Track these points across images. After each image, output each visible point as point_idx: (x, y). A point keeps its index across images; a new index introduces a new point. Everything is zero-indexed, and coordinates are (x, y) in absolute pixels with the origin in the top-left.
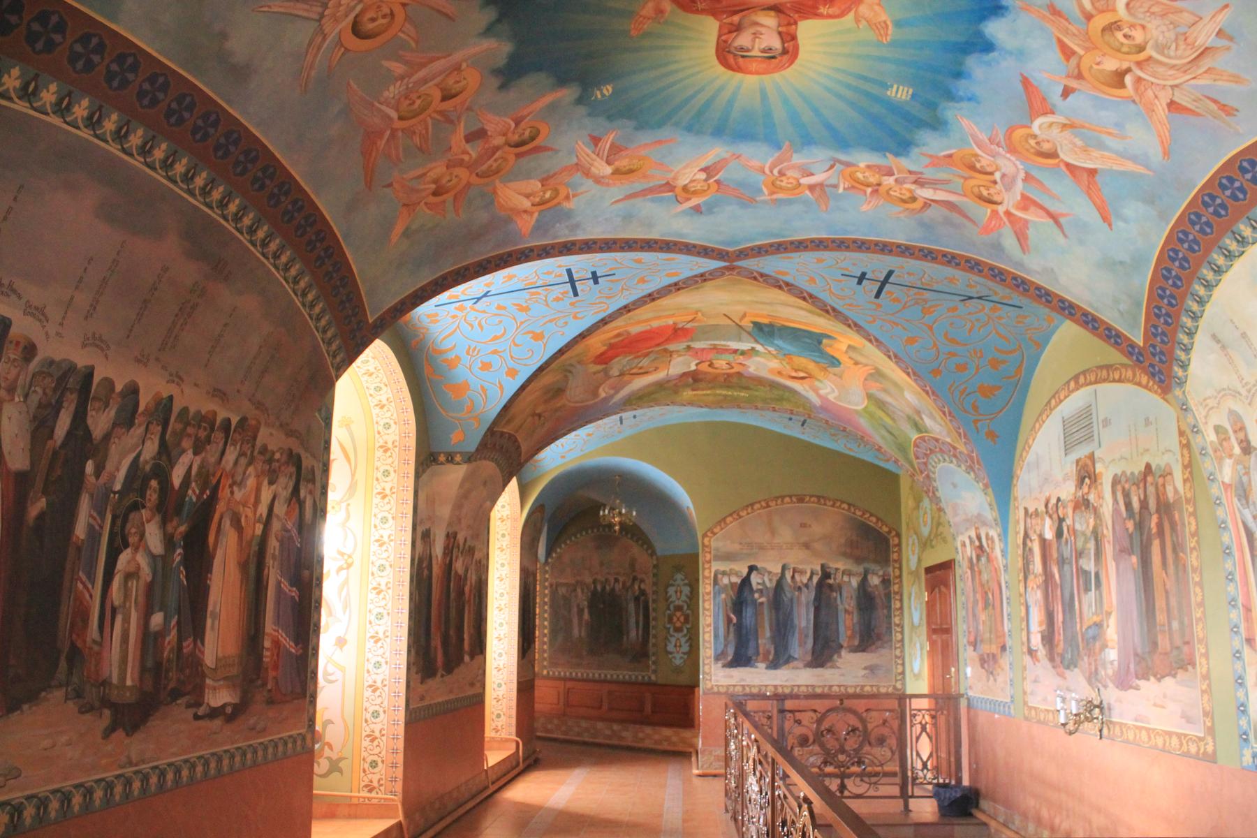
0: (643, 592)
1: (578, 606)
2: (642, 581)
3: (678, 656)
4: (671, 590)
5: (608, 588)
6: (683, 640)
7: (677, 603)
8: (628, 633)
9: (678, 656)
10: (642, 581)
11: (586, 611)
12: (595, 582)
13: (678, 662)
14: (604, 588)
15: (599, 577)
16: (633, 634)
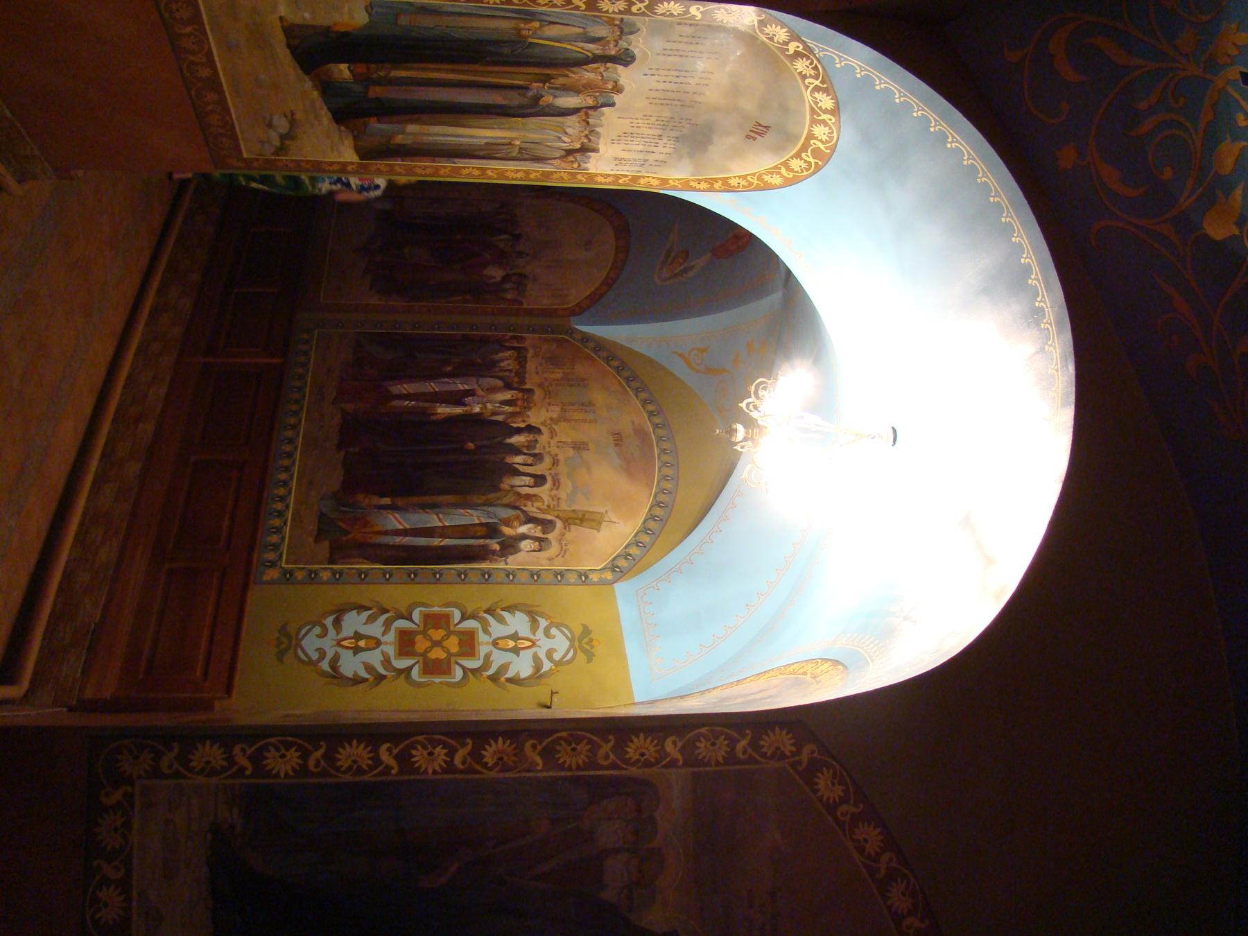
0: (509, 546)
1: (471, 393)
2: (542, 543)
3: (544, 644)
4: (351, 665)
5: (519, 459)
6: (497, 629)
7: (391, 650)
8: (393, 508)
9: (328, 644)
10: (542, 543)
11: (459, 410)
12: (530, 429)
13: (311, 643)
14: (517, 451)
15: (543, 439)
16: (395, 521)
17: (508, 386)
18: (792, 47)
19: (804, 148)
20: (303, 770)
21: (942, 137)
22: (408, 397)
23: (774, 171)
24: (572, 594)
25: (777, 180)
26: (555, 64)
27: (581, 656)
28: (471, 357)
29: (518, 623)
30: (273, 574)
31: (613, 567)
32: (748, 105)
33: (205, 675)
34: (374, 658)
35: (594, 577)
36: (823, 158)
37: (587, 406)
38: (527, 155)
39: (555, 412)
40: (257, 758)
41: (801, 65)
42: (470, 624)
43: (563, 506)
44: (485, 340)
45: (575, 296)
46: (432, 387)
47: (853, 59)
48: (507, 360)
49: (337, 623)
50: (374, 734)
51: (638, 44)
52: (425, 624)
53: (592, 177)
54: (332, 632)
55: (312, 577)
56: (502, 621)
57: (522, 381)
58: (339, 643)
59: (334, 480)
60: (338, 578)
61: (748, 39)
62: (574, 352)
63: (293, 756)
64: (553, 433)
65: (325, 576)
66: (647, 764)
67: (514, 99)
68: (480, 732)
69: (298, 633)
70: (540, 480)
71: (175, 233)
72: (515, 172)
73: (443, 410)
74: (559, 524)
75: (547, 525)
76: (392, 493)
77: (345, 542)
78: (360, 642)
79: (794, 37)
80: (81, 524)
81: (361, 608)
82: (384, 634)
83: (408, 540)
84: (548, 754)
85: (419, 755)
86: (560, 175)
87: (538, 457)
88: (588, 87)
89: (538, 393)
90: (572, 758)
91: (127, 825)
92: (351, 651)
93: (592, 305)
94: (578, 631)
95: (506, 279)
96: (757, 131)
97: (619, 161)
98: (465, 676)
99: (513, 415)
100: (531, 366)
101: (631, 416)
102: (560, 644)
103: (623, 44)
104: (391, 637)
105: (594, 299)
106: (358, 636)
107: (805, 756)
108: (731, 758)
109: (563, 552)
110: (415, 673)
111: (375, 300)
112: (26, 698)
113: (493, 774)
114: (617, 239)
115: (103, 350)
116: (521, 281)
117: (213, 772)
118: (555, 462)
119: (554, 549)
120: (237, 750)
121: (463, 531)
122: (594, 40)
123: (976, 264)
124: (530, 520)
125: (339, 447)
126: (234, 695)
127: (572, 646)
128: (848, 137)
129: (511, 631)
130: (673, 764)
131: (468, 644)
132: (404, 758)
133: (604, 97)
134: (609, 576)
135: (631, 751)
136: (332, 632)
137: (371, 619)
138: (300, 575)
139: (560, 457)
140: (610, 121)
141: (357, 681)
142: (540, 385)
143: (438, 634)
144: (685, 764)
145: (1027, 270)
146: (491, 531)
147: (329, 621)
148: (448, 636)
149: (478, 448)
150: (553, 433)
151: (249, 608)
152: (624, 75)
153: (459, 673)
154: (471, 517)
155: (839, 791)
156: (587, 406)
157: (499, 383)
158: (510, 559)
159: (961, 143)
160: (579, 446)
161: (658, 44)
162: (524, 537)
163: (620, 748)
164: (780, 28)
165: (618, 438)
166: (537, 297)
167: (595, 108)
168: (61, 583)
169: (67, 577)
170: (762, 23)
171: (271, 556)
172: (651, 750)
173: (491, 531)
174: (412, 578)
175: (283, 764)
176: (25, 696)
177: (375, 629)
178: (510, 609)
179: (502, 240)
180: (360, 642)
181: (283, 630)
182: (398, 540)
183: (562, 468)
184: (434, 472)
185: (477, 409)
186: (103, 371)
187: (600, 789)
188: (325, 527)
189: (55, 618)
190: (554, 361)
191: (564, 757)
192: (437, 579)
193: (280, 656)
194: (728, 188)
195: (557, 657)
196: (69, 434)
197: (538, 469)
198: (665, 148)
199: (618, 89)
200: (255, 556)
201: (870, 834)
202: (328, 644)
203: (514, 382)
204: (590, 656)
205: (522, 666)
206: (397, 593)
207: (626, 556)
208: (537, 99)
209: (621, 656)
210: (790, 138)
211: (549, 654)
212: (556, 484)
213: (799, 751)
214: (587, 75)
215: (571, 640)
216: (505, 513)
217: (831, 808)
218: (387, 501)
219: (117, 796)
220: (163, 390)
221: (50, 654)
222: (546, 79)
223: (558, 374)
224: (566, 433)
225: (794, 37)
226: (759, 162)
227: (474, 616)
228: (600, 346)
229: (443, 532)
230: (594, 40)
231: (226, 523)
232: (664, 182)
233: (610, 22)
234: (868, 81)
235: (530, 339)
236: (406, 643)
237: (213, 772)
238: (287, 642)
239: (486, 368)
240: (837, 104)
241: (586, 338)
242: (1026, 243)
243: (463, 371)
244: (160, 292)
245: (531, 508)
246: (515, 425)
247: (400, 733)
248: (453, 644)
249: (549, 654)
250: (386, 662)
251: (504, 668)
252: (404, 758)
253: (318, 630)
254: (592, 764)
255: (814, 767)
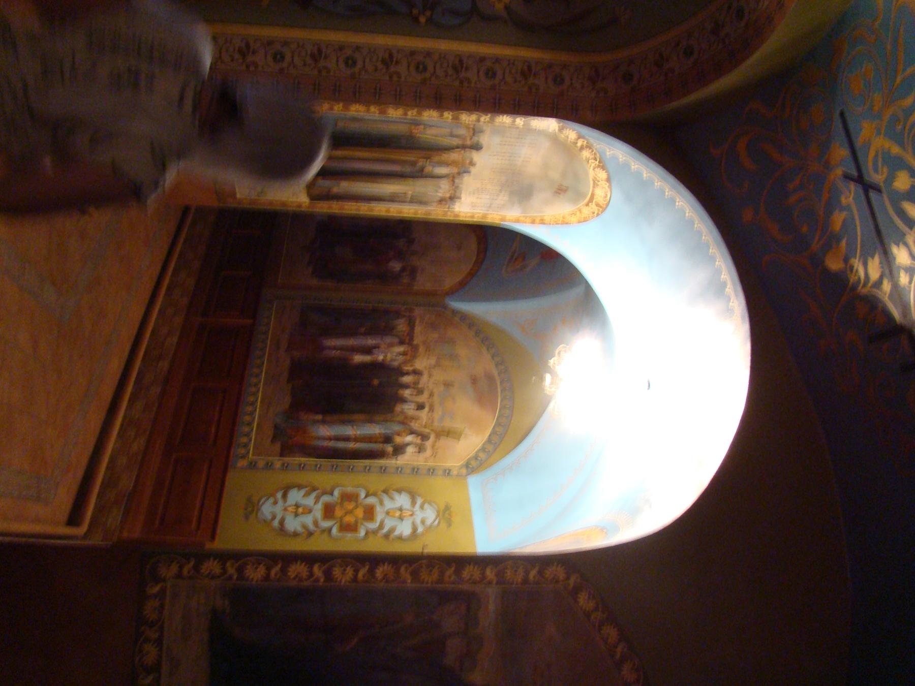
0: (399, 450)
1: (377, 347)
2: (421, 449)
3: (419, 516)
4: (292, 524)
8: (324, 422)
9: (278, 509)
12: (416, 373)
13: (267, 509)
14: (406, 386)
15: (424, 379)
16: (324, 431)
17: (402, 343)
18: (580, 143)
19: (591, 200)
20: (267, 578)
21: (673, 201)
22: (335, 348)
23: (574, 214)
24: (438, 482)
25: (574, 219)
26: (433, 150)
27: (443, 525)
28: (378, 322)
29: (403, 500)
30: (242, 463)
31: (467, 465)
32: (555, 175)
33: (198, 528)
34: (308, 520)
35: (454, 472)
36: (602, 208)
37: (453, 357)
38: (415, 200)
39: (433, 361)
40: (240, 570)
41: (586, 154)
42: (371, 500)
43: (436, 424)
44: (387, 312)
45: (449, 283)
46: (351, 342)
47: (618, 152)
48: (401, 325)
49: (285, 496)
50: (310, 559)
51: (484, 139)
52: (342, 499)
53: (457, 216)
54: (280, 502)
55: (269, 466)
56: (392, 498)
57: (412, 339)
58: (285, 509)
59: (287, 401)
60: (285, 467)
61: (554, 139)
62: (446, 319)
63: (261, 571)
64: (430, 376)
65: (278, 464)
66: (475, 583)
67: (408, 169)
68: (374, 560)
69: (259, 501)
70: (421, 407)
71: (183, 235)
72: (408, 211)
73: (358, 358)
74: (432, 437)
75: (425, 437)
76: (324, 412)
77: (290, 443)
78: (298, 509)
79: (580, 137)
80: (122, 425)
81: (300, 487)
82: (315, 503)
83: (332, 444)
84: (415, 574)
85: (337, 572)
86: (437, 213)
87: (420, 392)
88: (454, 163)
89: (421, 349)
90: (429, 578)
91: (162, 607)
92: (293, 512)
93: (461, 288)
94: (442, 507)
95: (403, 269)
96: (560, 190)
97: (473, 205)
98: (366, 534)
99: (405, 362)
100: (418, 329)
101: (484, 364)
102: (430, 515)
103: (475, 139)
104: (320, 506)
105: (462, 285)
106: (297, 506)
107: (572, 581)
108: (525, 581)
109: (434, 455)
110: (335, 531)
111: (315, 282)
112: (85, 536)
113: (382, 584)
114: (479, 243)
115: (137, 313)
116: (413, 272)
117: (213, 577)
118: (431, 395)
119: (428, 452)
120: (228, 564)
121: (370, 439)
122: (457, 136)
123: (699, 276)
124: (412, 432)
125: (288, 381)
126: (217, 539)
127: (438, 516)
128: (617, 197)
129: (398, 505)
130: (490, 583)
131: (370, 513)
132: (328, 574)
133: (464, 169)
134: (464, 471)
135: (466, 574)
136: (280, 502)
137: (307, 495)
138: (261, 464)
139: (435, 391)
140: (468, 182)
141: (296, 534)
142: (424, 342)
143: (350, 506)
144: (497, 583)
145: (724, 285)
146: (388, 439)
147: (279, 495)
148: (356, 507)
149: (380, 384)
150: (430, 376)
151: (227, 483)
152: (476, 156)
153: (362, 533)
154: (375, 430)
155: (592, 605)
156: (453, 357)
157: (396, 340)
158: (400, 457)
159: (683, 204)
160: (448, 385)
161: (497, 140)
162: (408, 444)
163: (458, 572)
164: (572, 132)
165: (474, 381)
166: (423, 283)
167: (459, 174)
168: (108, 464)
169: (112, 460)
170: (561, 130)
171: (242, 451)
172: (477, 574)
173: (388, 439)
174: (334, 469)
175: (255, 574)
176: (85, 534)
177: (310, 501)
178: (399, 491)
179: (401, 243)
180: (298, 509)
181: (249, 499)
182: (326, 444)
183: (436, 399)
184: (352, 405)
185: (381, 358)
186: (137, 326)
187: (446, 597)
188: (278, 433)
189: (105, 486)
190: (433, 326)
191: (424, 575)
192: (350, 470)
193: (247, 517)
194: (542, 222)
195: (428, 522)
196: (116, 366)
197: (422, 398)
198: (503, 198)
199: (472, 164)
200: (232, 450)
201: (611, 633)
202: (278, 509)
203: (407, 340)
204: (449, 524)
205: (405, 529)
206: (323, 479)
207: (476, 457)
208: (422, 170)
209: (469, 523)
210: (583, 196)
211: (423, 522)
212: (432, 409)
213: (568, 578)
214: (454, 156)
215: (438, 512)
216: (397, 428)
217: (588, 615)
218: (319, 417)
219: (156, 589)
220: (175, 339)
221: (101, 509)
222: (427, 158)
223: (435, 335)
224: (439, 376)
225: (580, 137)
226: (563, 208)
227: (375, 494)
228: (464, 317)
229: (356, 439)
230: (457, 136)
231: (213, 430)
232: (503, 219)
233: (468, 127)
234: (626, 165)
235: (417, 312)
236: (329, 511)
237: (213, 577)
238: (252, 507)
239: (388, 330)
240: (608, 175)
241: (455, 312)
242: (723, 267)
243: (373, 331)
244: (173, 275)
245: (415, 425)
246: (406, 368)
247: (326, 559)
248: (360, 513)
249: (423, 522)
250: (316, 523)
251: (392, 530)
252: (328, 574)
253: (271, 500)
254: (440, 581)
255: (576, 591)
